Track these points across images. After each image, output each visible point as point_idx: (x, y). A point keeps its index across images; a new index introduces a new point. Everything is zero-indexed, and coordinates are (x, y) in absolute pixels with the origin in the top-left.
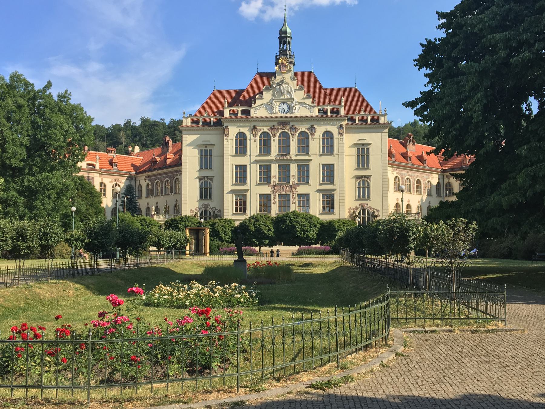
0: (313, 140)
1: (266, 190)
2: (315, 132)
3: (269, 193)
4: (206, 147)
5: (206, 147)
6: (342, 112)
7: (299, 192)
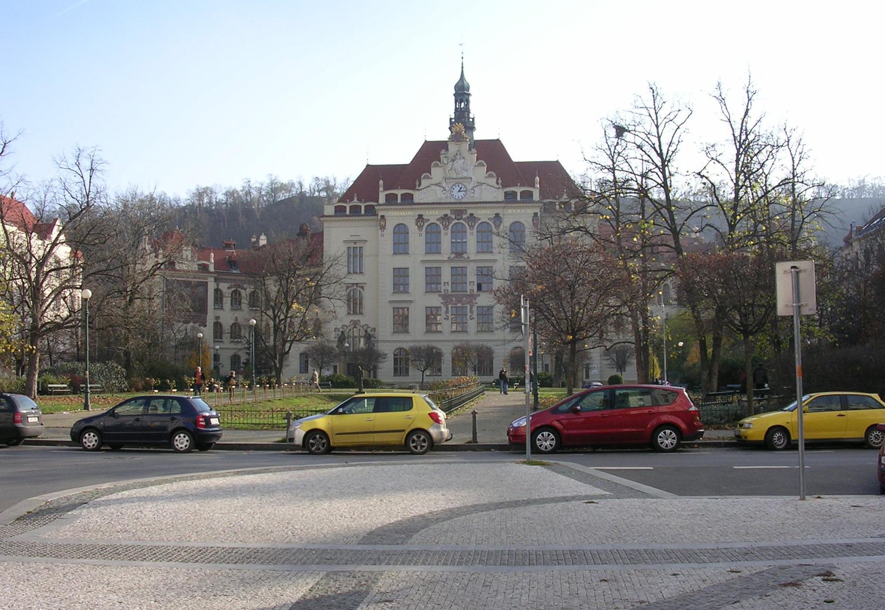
1: (435, 300)
4: (355, 243)
5: (355, 243)
6: (536, 196)
7: (480, 304)
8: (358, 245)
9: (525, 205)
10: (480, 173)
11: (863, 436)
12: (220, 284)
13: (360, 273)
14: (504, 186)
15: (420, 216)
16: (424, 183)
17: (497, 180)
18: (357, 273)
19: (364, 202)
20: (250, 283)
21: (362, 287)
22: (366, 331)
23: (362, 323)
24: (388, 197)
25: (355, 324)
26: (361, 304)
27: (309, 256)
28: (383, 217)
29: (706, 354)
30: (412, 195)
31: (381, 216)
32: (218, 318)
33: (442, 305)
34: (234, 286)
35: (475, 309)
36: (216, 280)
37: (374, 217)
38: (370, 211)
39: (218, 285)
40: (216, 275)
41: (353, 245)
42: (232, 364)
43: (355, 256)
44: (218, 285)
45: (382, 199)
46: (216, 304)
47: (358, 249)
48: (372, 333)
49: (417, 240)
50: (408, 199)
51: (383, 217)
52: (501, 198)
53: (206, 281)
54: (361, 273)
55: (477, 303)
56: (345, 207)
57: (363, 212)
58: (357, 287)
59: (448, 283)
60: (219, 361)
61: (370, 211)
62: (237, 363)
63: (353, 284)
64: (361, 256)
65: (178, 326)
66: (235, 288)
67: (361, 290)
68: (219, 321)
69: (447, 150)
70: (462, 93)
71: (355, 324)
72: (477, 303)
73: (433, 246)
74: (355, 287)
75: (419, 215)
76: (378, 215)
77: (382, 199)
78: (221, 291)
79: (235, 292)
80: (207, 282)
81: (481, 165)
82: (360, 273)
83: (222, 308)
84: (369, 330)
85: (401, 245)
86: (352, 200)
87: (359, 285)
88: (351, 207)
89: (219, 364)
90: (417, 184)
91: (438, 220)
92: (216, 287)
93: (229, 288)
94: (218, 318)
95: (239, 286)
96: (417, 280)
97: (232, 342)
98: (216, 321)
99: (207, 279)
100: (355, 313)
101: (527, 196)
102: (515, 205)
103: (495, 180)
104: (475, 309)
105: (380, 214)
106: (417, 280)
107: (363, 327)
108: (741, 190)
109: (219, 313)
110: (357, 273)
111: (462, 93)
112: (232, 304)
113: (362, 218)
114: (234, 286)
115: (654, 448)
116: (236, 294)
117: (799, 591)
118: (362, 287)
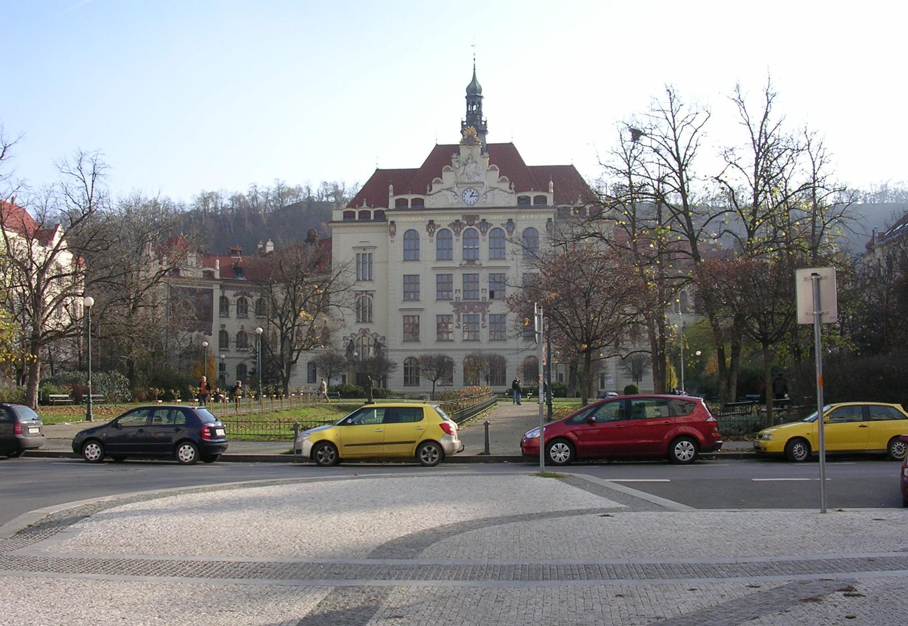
1: (447, 308)
4: (364, 250)
5: (364, 250)
6: (550, 201)
7: (492, 312)
8: (367, 252)
9: (538, 210)
10: (492, 177)
11: (886, 448)
12: (226, 291)
13: (369, 280)
14: (517, 191)
15: (431, 222)
16: (435, 187)
17: (510, 185)
18: (366, 280)
19: (374, 208)
20: (256, 291)
21: (372, 295)
22: (376, 340)
23: (372, 332)
24: (398, 202)
25: (364, 332)
27: (317, 263)
28: (393, 222)
29: (724, 364)
30: (423, 200)
31: (391, 222)
32: (223, 326)
33: (454, 313)
34: (241, 294)
35: (487, 317)
36: (222, 287)
37: (384, 223)
38: (380, 216)
39: (223, 292)
40: (221, 282)
41: (362, 252)
42: (238, 373)
43: (364, 263)
44: (223, 292)
45: (392, 204)
46: (222, 312)
47: (368, 255)
48: (382, 342)
49: (428, 246)
50: (418, 205)
51: (393, 222)
52: (514, 203)
53: (211, 288)
54: (371, 280)
55: (489, 311)
56: (354, 212)
57: (372, 218)
58: (366, 294)
59: (459, 290)
60: (225, 370)
61: (380, 216)
62: (243, 373)
63: (362, 291)
64: (371, 263)
65: (182, 334)
66: (241, 296)
67: (371, 297)
68: (225, 329)
69: (459, 154)
70: (474, 95)
71: (364, 332)
72: (489, 311)
74: (364, 295)
75: (430, 221)
76: (387, 221)
77: (392, 204)
78: (227, 299)
79: (241, 299)
80: (212, 290)
81: (493, 169)
82: (369, 280)
83: (227, 316)
84: (378, 339)
85: (411, 252)
86: (361, 205)
87: (369, 292)
88: (360, 213)
89: (225, 374)
90: (428, 189)
91: (449, 225)
92: (222, 295)
93: (235, 296)
94: (223, 326)
95: (245, 294)
96: (428, 287)
97: (238, 351)
98: (221, 329)
99: (212, 286)
100: (364, 321)
101: (541, 201)
102: (529, 210)
103: (508, 185)
104: (487, 317)
105: (390, 219)
106: (428, 287)
107: (372, 335)
109: (225, 321)
110: (366, 280)
111: (474, 95)
112: (238, 312)
113: (371, 224)
114: (241, 294)
115: (671, 460)
116: (242, 302)
117: (820, 607)
118: (372, 295)
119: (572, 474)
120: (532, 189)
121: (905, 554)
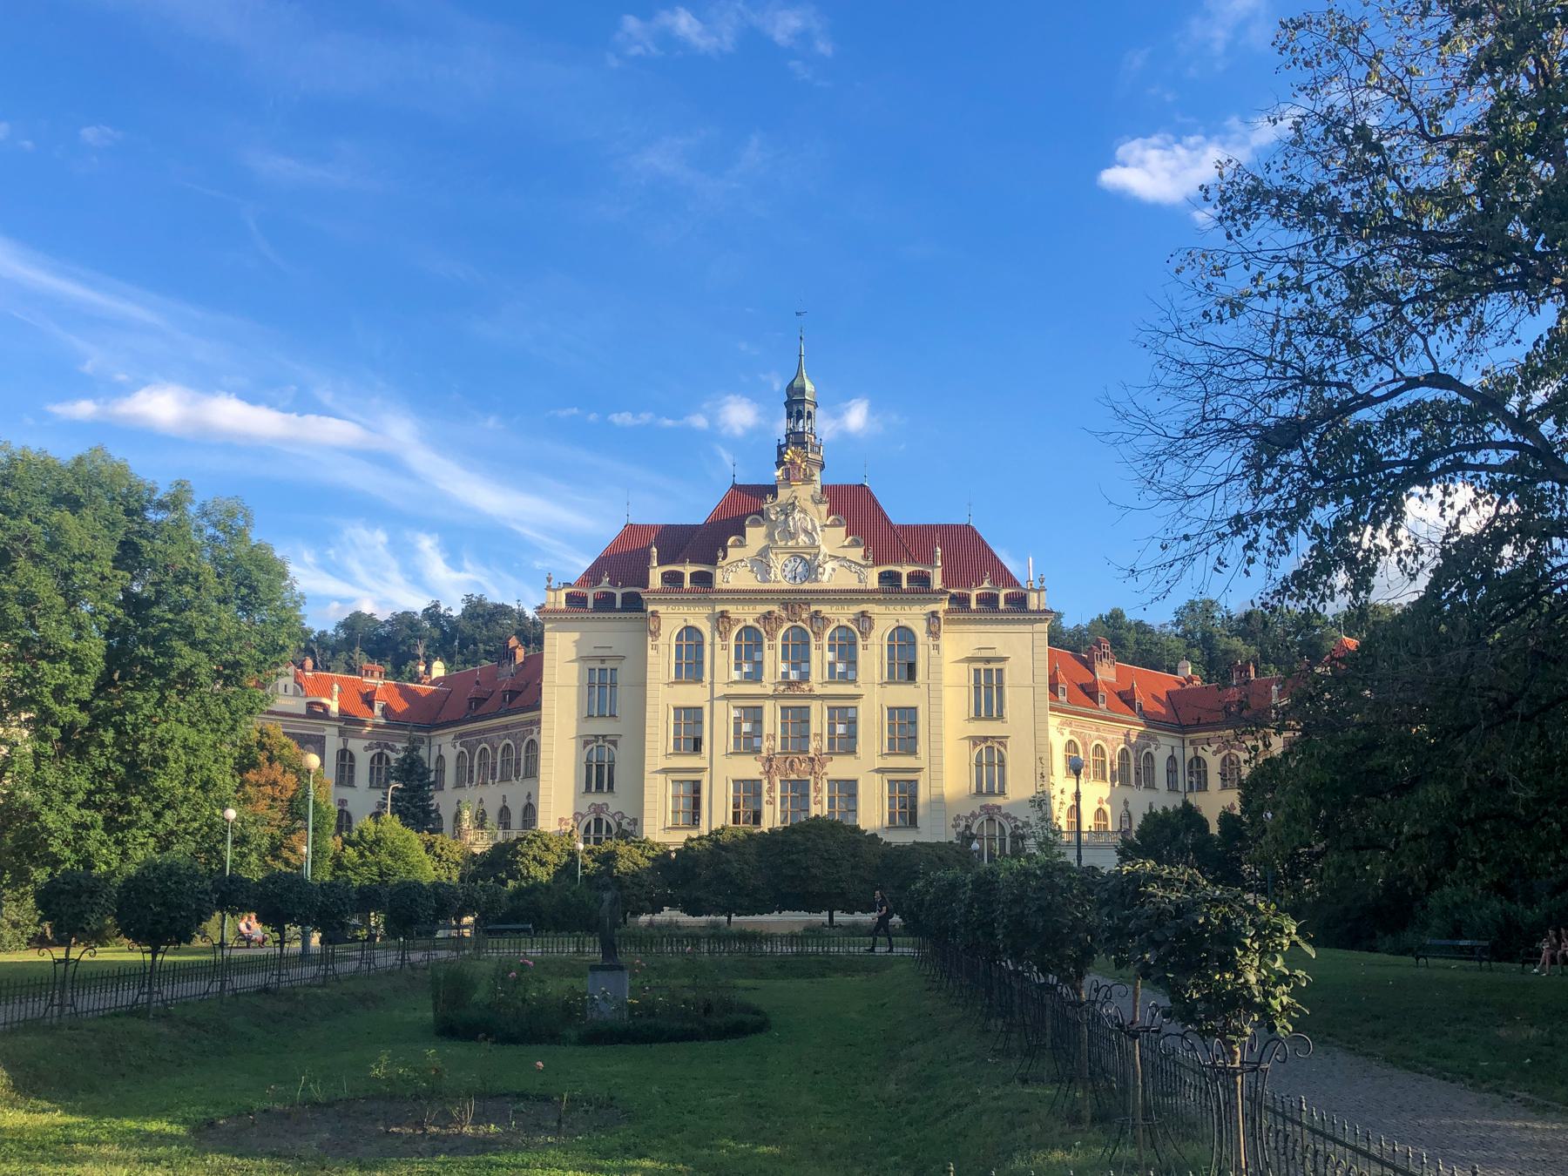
0: (865, 647)
1: (750, 768)
2: (871, 628)
3: (757, 776)
4: (603, 661)
5: (603, 661)
6: (937, 583)
7: (831, 776)
8: (608, 665)
9: (918, 596)
10: (832, 541)
13: (611, 716)
14: (877, 563)
15: (723, 614)
16: (733, 553)
18: (605, 716)
19: (622, 587)
21: (614, 743)
22: (619, 825)
23: (612, 810)
24: (667, 578)
26: (372, 769)
28: (654, 614)
31: (652, 612)
32: (342, 802)
33: (762, 777)
34: (378, 745)
36: (342, 733)
37: (639, 615)
38: (634, 604)
40: (342, 724)
41: (597, 665)
43: (602, 686)
47: (609, 671)
48: (629, 828)
49: (721, 659)
50: (703, 580)
52: (872, 579)
53: (322, 734)
54: (613, 716)
55: (826, 774)
57: (618, 605)
58: (604, 741)
63: (596, 736)
64: (614, 685)
66: (379, 750)
67: (612, 747)
68: (346, 808)
69: (775, 496)
72: (826, 774)
73: (845, 716)
74: (600, 742)
76: (646, 611)
78: (351, 756)
80: (324, 737)
82: (611, 716)
84: (624, 822)
85: (691, 665)
86: (597, 582)
87: (608, 738)
90: (721, 554)
91: (757, 621)
92: (342, 747)
93: (366, 749)
94: (342, 802)
96: (720, 727)
99: (324, 730)
101: (921, 580)
102: (899, 597)
103: (861, 551)
105: (650, 608)
106: (720, 727)
107: (613, 817)
108: (1535, 407)
109: (346, 793)
110: (605, 716)
113: (617, 615)
114: (378, 745)
118: (614, 743)
119: (1529, 1124)
120: (673, 855)
121: (1214, 1172)
